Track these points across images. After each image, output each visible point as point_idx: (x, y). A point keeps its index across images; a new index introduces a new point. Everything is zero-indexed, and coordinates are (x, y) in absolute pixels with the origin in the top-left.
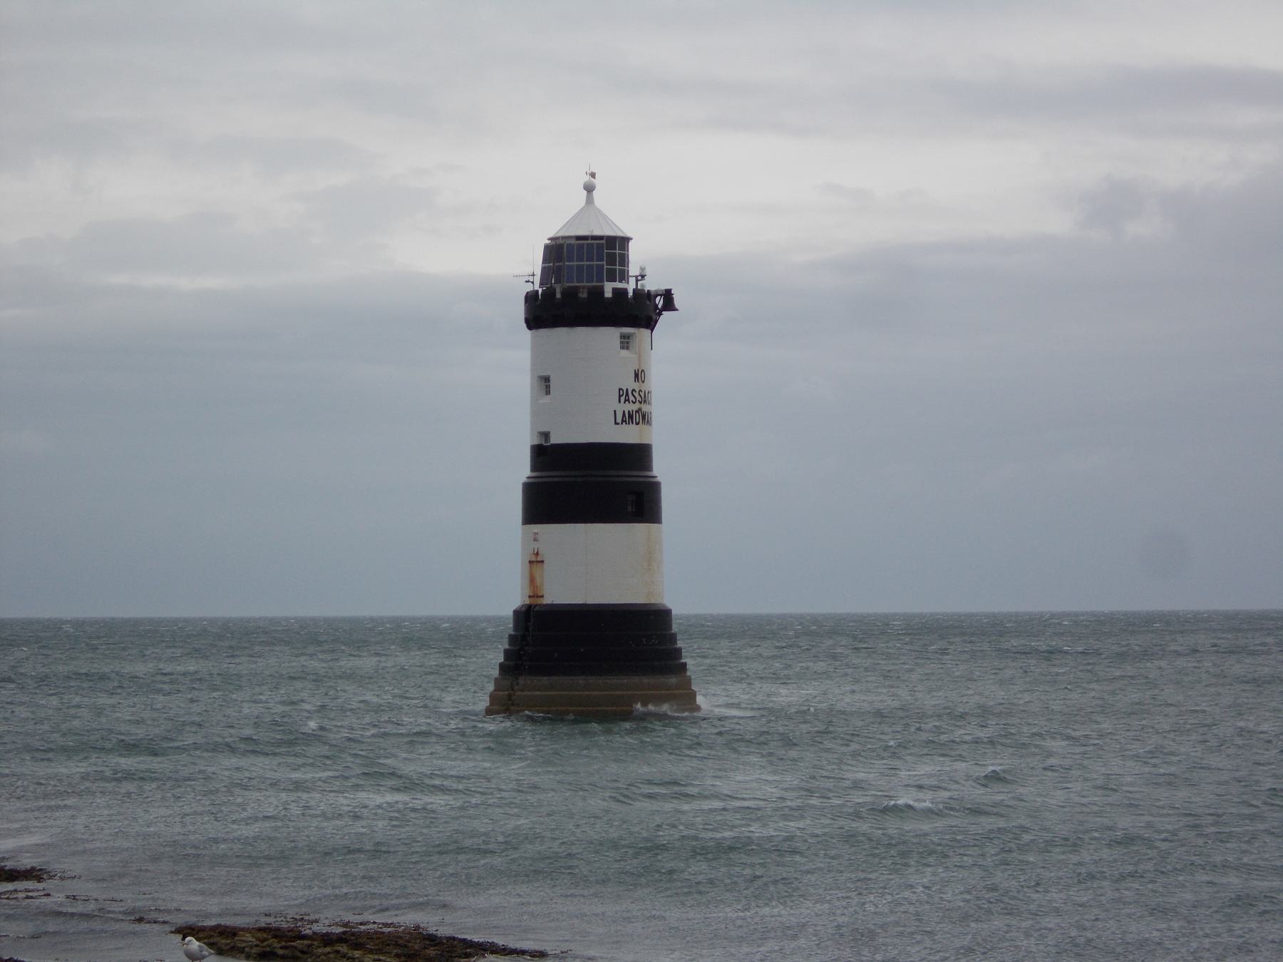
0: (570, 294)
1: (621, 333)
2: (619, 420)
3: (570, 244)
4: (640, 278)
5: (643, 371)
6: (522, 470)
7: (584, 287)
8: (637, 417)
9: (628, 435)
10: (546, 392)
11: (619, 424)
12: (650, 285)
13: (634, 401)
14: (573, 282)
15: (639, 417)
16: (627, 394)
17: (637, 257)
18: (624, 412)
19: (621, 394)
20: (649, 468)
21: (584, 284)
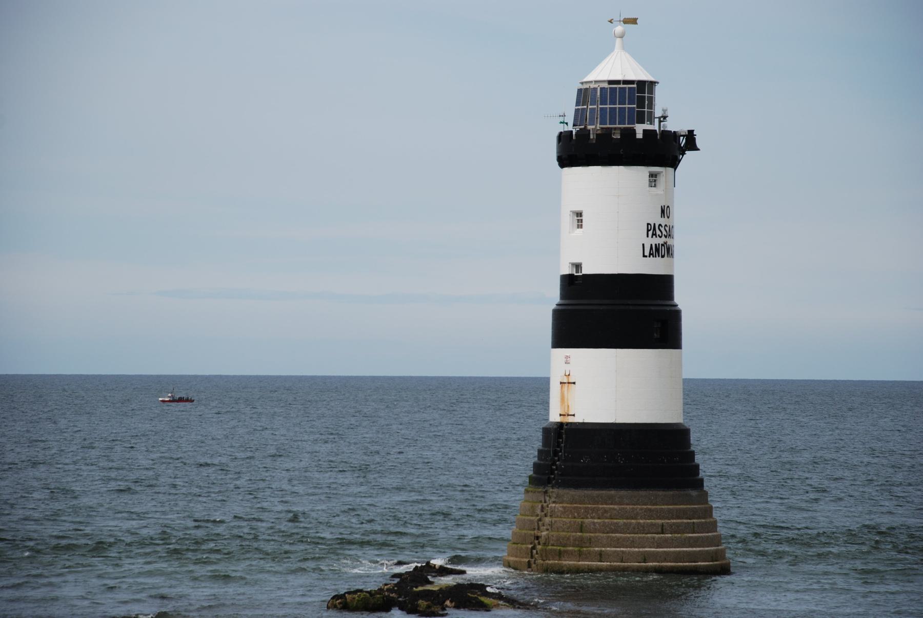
0: (605, 135)
1: (650, 172)
2: (647, 253)
3: (604, 88)
4: (662, 119)
5: (668, 207)
6: (553, 296)
7: (615, 129)
8: (663, 250)
10: (578, 225)
11: (646, 256)
12: (671, 125)
15: (662, 251)
17: (661, 101)
18: (651, 245)
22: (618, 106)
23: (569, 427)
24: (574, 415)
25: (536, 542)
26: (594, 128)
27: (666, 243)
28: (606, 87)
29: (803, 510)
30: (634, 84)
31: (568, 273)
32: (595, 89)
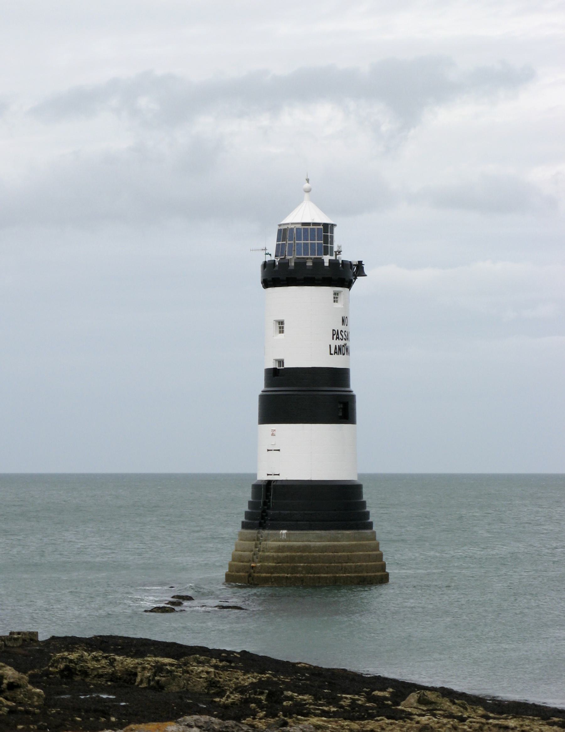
0: (300, 264)
1: (334, 291)
2: (333, 352)
3: (299, 228)
4: (337, 253)
5: (346, 317)
7: (307, 258)
8: (344, 350)
9: (336, 362)
11: (332, 354)
13: (342, 338)
14: (302, 255)
16: (338, 334)
18: (336, 346)
19: (334, 333)
20: (348, 385)
21: (309, 256)
22: (316, 242)
23: (274, 484)
24: (279, 475)
25: (252, 571)
26: (292, 258)
27: (346, 345)
28: (300, 227)
29: (81, 542)
30: (320, 226)
31: (272, 367)
32: (292, 229)
